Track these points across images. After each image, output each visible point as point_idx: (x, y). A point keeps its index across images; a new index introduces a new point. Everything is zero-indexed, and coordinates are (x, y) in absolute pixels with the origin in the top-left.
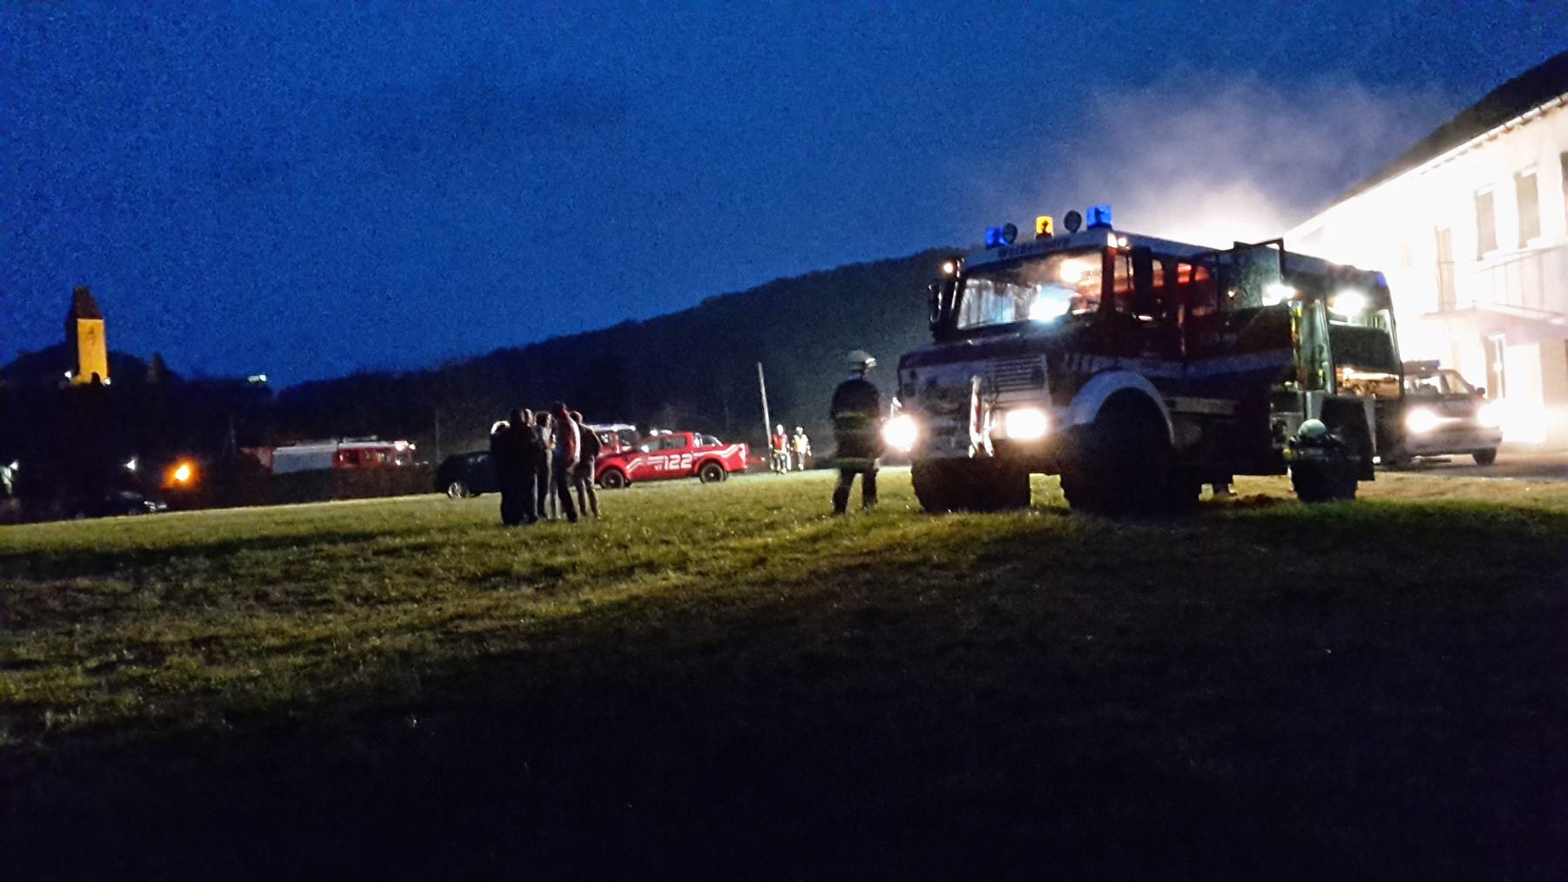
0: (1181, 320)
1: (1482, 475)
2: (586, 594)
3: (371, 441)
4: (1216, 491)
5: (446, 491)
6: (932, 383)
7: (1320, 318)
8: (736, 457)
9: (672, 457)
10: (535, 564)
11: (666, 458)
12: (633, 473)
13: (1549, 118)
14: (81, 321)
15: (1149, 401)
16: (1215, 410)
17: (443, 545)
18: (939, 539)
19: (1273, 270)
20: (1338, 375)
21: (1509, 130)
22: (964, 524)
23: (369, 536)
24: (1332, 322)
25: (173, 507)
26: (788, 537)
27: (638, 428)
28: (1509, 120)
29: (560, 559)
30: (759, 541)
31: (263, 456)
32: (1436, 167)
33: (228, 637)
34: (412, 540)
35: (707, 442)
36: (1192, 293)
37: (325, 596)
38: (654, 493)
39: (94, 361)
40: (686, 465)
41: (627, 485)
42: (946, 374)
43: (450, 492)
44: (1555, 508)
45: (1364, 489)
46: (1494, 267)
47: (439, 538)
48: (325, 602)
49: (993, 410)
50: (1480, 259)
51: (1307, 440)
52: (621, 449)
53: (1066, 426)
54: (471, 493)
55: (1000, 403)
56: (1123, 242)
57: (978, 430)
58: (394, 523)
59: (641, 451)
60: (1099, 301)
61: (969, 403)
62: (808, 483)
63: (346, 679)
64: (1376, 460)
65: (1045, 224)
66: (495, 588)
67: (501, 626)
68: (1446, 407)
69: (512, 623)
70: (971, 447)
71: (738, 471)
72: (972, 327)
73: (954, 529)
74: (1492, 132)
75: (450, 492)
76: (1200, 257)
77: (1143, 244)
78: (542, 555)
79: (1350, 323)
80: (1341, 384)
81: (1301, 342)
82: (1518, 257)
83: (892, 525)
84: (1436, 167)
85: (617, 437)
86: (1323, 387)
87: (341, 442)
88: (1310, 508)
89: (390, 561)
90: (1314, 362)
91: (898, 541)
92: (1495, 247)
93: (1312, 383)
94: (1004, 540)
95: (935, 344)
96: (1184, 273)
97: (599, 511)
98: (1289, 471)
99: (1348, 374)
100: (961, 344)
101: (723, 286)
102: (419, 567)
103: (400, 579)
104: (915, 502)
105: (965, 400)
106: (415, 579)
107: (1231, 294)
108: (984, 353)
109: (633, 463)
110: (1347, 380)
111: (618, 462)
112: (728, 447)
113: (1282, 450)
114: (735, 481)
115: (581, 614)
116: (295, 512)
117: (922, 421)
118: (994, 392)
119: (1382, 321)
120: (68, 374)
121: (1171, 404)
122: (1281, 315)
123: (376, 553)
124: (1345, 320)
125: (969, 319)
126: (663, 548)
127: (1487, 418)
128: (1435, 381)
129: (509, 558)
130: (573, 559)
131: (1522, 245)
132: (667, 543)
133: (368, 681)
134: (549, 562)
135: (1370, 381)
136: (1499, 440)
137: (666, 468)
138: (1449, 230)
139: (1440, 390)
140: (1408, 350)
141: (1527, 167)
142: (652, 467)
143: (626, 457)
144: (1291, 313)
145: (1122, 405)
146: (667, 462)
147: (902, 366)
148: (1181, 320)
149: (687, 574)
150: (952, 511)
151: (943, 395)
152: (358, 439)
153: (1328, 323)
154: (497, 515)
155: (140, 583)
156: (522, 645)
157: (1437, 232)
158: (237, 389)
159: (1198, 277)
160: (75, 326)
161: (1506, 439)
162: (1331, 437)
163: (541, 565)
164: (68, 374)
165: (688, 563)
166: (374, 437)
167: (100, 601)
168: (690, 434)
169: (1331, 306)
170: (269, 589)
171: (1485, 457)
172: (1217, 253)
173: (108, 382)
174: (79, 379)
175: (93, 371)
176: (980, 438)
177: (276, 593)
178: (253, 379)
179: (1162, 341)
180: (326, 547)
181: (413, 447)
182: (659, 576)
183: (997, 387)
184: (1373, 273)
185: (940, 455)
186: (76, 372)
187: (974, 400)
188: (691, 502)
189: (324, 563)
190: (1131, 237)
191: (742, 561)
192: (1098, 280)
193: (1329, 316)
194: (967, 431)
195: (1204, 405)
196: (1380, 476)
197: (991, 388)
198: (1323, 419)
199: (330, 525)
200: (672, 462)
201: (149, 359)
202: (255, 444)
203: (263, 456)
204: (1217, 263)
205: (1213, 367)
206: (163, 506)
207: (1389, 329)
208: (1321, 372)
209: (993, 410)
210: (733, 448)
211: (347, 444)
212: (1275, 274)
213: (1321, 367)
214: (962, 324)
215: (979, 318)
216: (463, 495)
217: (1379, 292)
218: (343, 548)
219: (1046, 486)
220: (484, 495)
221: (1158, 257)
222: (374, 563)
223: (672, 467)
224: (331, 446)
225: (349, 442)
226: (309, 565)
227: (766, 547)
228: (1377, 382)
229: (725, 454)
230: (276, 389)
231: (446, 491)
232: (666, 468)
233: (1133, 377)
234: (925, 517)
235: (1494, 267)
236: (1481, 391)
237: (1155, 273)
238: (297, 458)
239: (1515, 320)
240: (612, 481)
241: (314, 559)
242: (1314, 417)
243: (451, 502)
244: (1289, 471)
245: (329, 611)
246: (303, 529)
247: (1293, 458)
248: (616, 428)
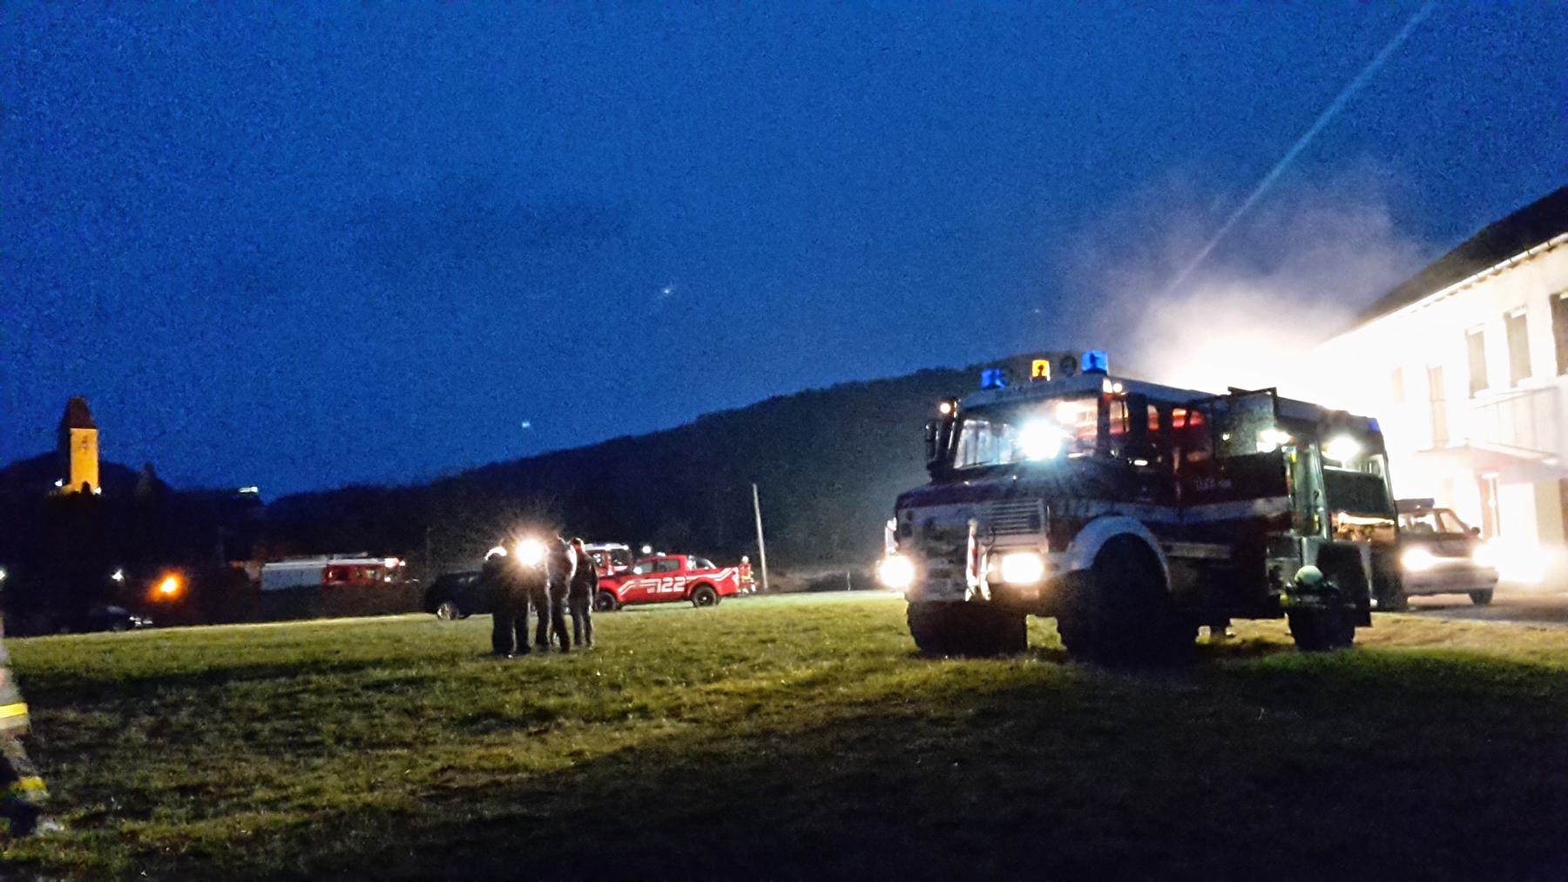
0: (1176, 465)
1: (1479, 617)
2: (579, 742)
4: (1213, 631)
5: (435, 612)
6: (929, 524)
7: (1314, 464)
8: (729, 580)
9: (666, 579)
10: (526, 705)
11: (659, 580)
12: (624, 596)
13: (1537, 260)
15: (1141, 542)
16: (1214, 555)
17: (434, 680)
18: (934, 690)
19: (1267, 418)
20: (1334, 519)
21: (1497, 273)
22: (960, 672)
23: (357, 666)
24: (1326, 467)
25: (158, 624)
26: (783, 681)
27: (631, 547)
28: (1498, 263)
29: (552, 702)
30: (754, 684)
31: (251, 569)
32: (1426, 306)
33: (217, 785)
34: (401, 673)
35: (700, 565)
36: (1187, 438)
37: (317, 738)
38: (647, 617)
39: (85, 470)
40: (679, 589)
41: (619, 608)
42: (943, 514)
44: (1553, 664)
45: (1361, 634)
46: (1485, 406)
47: (429, 671)
48: (315, 744)
49: (990, 553)
50: (1472, 397)
51: (1303, 587)
52: (613, 569)
53: (1062, 572)
54: (461, 613)
55: (997, 546)
56: (1118, 388)
57: (975, 573)
58: (385, 651)
59: (633, 574)
60: (1094, 444)
61: (965, 546)
62: (803, 610)
63: (338, 846)
64: (1374, 602)
65: (1041, 368)
66: (487, 731)
68: (1441, 547)
69: (502, 778)
70: (967, 591)
71: (731, 594)
72: (969, 467)
73: (951, 676)
74: (1482, 274)
76: (1195, 402)
77: (1140, 391)
78: (534, 697)
79: (1344, 469)
80: (1336, 529)
81: (1296, 486)
82: (1510, 396)
83: (889, 670)
84: (1426, 306)
85: (609, 557)
86: (1319, 532)
87: (332, 558)
88: (1307, 658)
89: (378, 697)
90: (1311, 508)
91: (894, 690)
92: (1486, 386)
93: (1308, 528)
94: (1000, 693)
95: (931, 484)
96: (1179, 417)
97: (593, 641)
98: (1286, 615)
99: (1343, 519)
100: (958, 485)
101: (718, 403)
102: (409, 705)
103: (390, 719)
104: (908, 642)
105: (961, 542)
106: (406, 720)
107: (1226, 437)
108: (983, 494)
109: (624, 586)
110: (1343, 524)
112: (722, 570)
113: (1279, 595)
114: (726, 603)
115: (575, 767)
116: (283, 632)
117: (918, 563)
118: (991, 535)
119: (1376, 467)
120: (59, 483)
121: (1167, 549)
122: (1275, 461)
123: (366, 687)
124: (1339, 465)
125: (965, 459)
126: (656, 690)
127: (1481, 558)
128: (1430, 519)
129: (502, 697)
130: (565, 700)
131: (1514, 385)
132: (661, 683)
133: (358, 849)
134: (539, 703)
135: (1366, 526)
136: (1495, 580)
137: (659, 591)
138: (1441, 367)
139: (1435, 528)
140: (1399, 491)
141: (1517, 308)
142: (645, 589)
143: (620, 577)
144: (1285, 458)
145: (1115, 552)
147: (899, 506)
148: (1176, 465)
149: (680, 721)
150: (949, 658)
151: (940, 537)
152: (346, 555)
153: (1322, 467)
154: (487, 644)
155: (129, 715)
156: (516, 809)
157: (1429, 371)
158: (233, 503)
159: (1193, 422)
160: (69, 436)
161: (1502, 579)
162: (1328, 585)
163: (533, 706)
164: (59, 483)
165: (683, 708)
166: (364, 554)
167: (86, 737)
168: (684, 557)
169: (1325, 450)
170: (257, 726)
171: (1482, 597)
172: (1213, 399)
173: (98, 491)
174: (69, 488)
175: (83, 480)
176: (977, 582)
177: (265, 729)
178: (244, 490)
179: (1158, 485)
180: (314, 677)
181: (403, 564)
182: (654, 723)
183: (993, 530)
184: (1364, 420)
185: (935, 597)
186: (67, 481)
187: (971, 543)
188: (683, 630)
189: (313, 698)
190: (1127, 383)
191: (736, 707)
192: (1092, 422)
193: (1323, 461)
194: (964, 575)
195: (1201, 551)
196: (1377, 617)
197: (991, 530)
198: (1319, 565)
199: (319, 653)
200: (665, 585)
201: (139, 468)
202: (246, 557)
203: (251, 569)
204: (1213, 411)
205: (1212, 512)
207: (1383, 474)
208: (1316, 518)
209: (990, 553)
210: (727, 572)
211: (337, 561)
212: (1268, 422)
213: (1317, 513)
214: (958, 465)
215: (975, 458)
216: (453, 617)
217: (1370, 434)
218: (335, 680)
219: (1043, 630)
220: (472, 616)
221: (1154, 402)
222: (364, 699)
224: (321, 562)
225: (337, 559)
226: (298, 700)
227: (760, 690)
228: (1372, 526)
229: (718, 577)
230: (268, 499)
231: (435, 612)
232: (659, 591)
233: (1126, 522)
234: (921, 662)
235: (1485, 406)
236: (1476, 531)
237: (1151, 417)
238: (288, 573)
239: (1509, 460)
240: (604, 604)
241: (303, 691)
242: (1309, 564)
243: (441, 624)
244: (1286, 615)
245: (319, 755)
246: (293, 656)
247: (1290, 604)
248: (609, 547)
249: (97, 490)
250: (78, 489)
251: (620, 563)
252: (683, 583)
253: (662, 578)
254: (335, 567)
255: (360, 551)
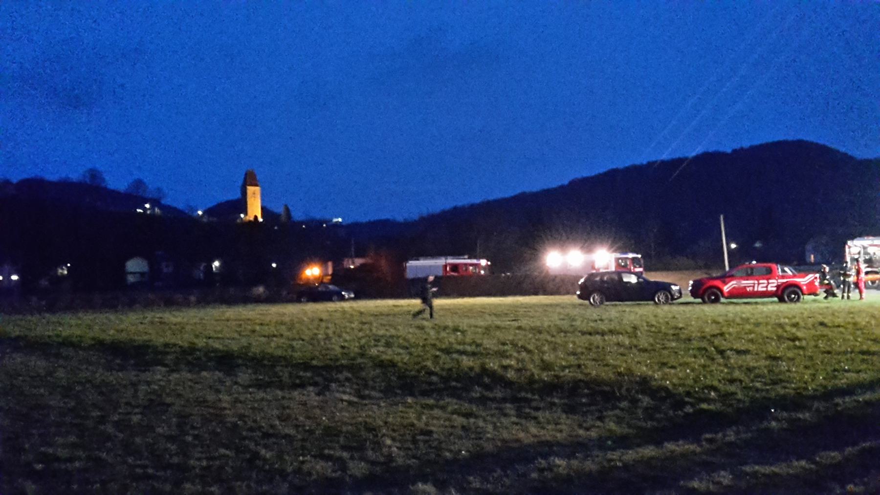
3: (465, 259)
8: (812, 283)
9: (761, 281)
11: (756, 282)
12: (729, 292)
14: (249, 188)
39: (255, 210)
43: (592, 300)
67: (538, 442)
75: (592, 300)
111: (717, 283)
142: (745, 287)
146: (756, 285)
166: (466, 257)
178: (335, 220)
200: (761, 285)
206: (352, 296)
210: (810, 277)
211: (451, 261)
223: (760, 289)
224: (441, 262)
248: (631, 255)
249: (261, 220)
250: (252, 219)
251: (637, 266)
252: (775, 285)
253: (758, 280)
254: (450, 264)
255: (463, 254)
